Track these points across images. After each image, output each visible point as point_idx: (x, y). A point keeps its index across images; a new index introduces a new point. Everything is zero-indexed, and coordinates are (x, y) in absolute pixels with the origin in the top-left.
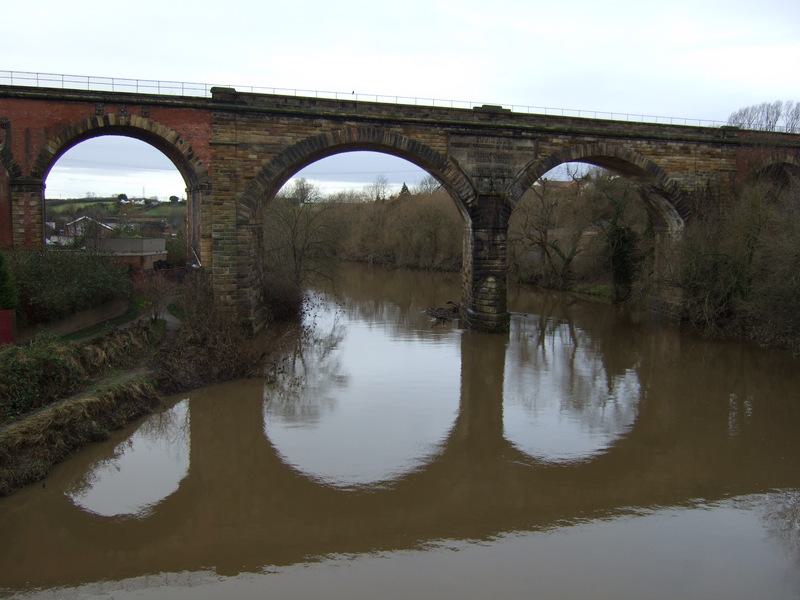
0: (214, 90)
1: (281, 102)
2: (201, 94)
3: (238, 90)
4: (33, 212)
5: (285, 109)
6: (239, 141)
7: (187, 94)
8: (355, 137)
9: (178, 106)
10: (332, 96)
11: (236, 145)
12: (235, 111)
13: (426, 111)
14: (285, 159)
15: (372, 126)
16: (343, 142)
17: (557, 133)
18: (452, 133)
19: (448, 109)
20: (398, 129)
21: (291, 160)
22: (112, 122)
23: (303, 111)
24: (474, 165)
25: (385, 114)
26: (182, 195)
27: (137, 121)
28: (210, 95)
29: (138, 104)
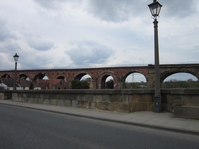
0: (148, 65)
1: (163, 66)
2: (147, 66)
3: (152, 64)
4: (121, 85)
5: (161, 67)
6: (153, 72)
7: (144, 66)
8: (175, 71)
9: (142, 68)
10: (170, 64)
11: (152, 73)
12: (152, 68)
13: (190, 65)
14: (161, 75)
15: (178, 69)
16: (172, 71)
17: (9, 92)
18: (196, 68)
19: (195, 64)
20: (184, 69)
21: (97, 87)
22: (132, 71)
23: (164, 67)
24: (88, 104)
25: (131, 67)
26: (145, 81)
27: (189, 69)
28: (148, 66)
29: (136, 68)
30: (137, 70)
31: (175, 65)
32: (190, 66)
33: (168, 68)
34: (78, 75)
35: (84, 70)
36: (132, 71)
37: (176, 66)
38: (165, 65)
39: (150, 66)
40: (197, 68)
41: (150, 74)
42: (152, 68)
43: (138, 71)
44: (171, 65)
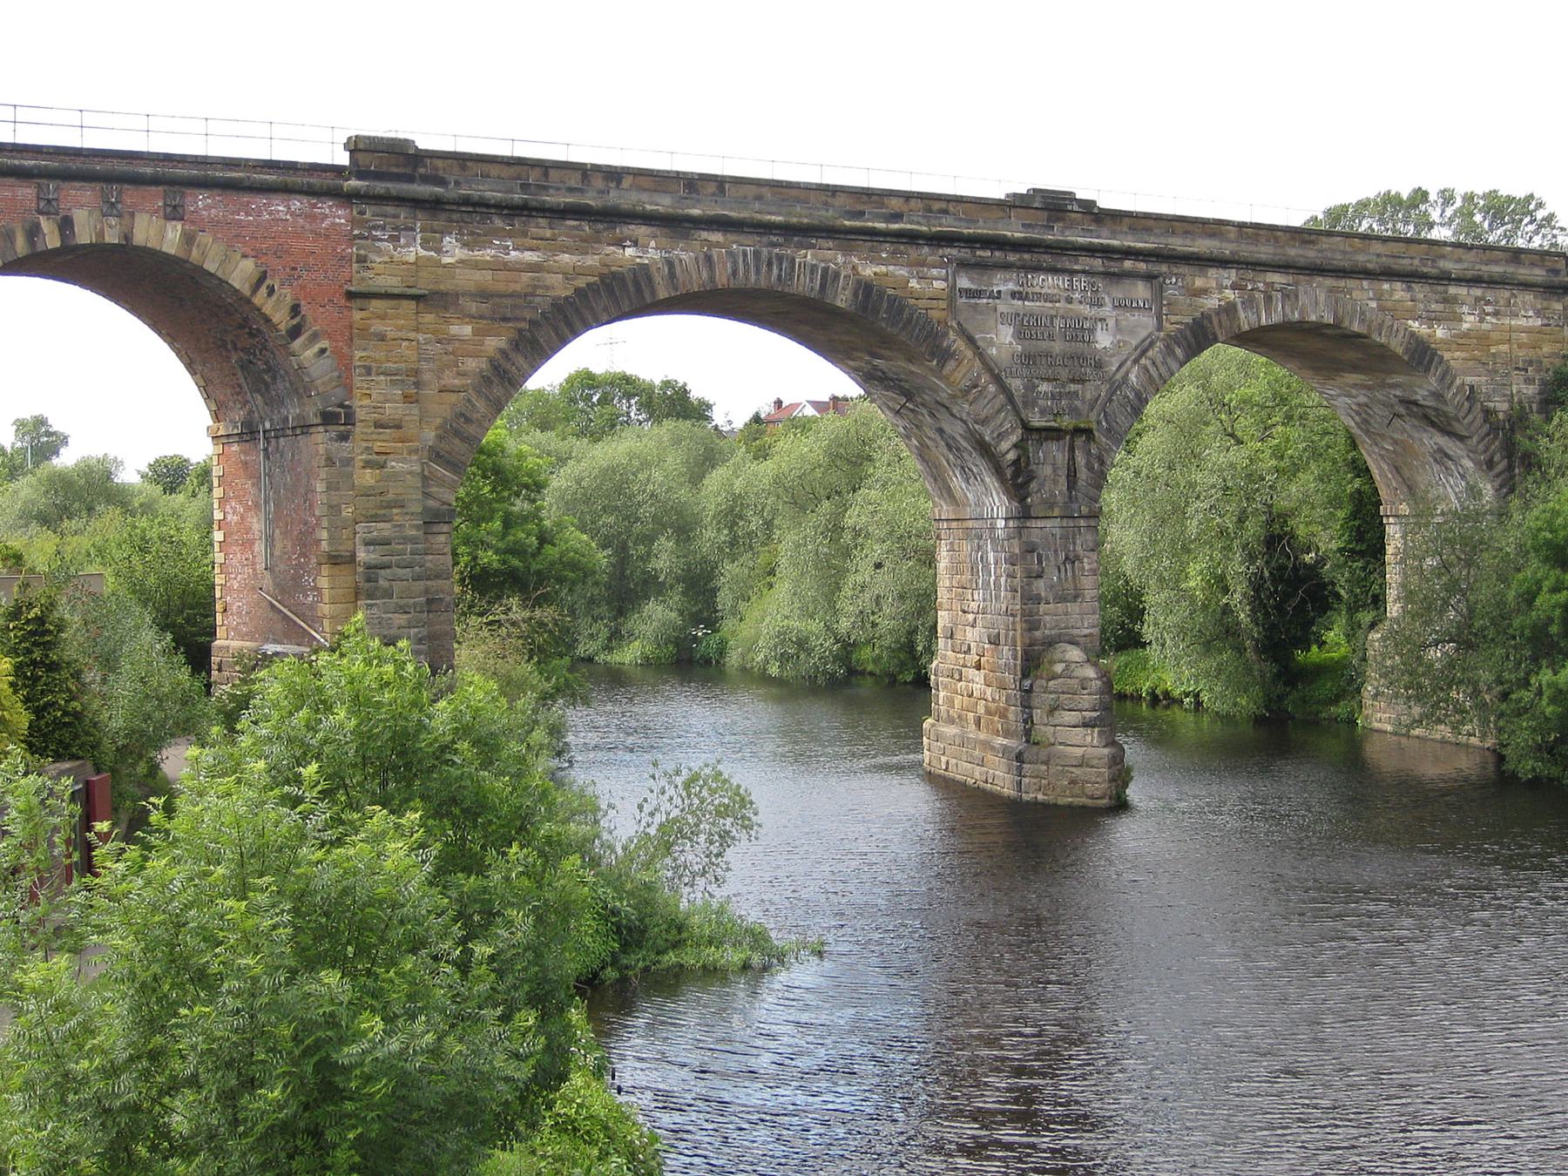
12: (416, 203)
13: (895, 203)
28: (343, 159)
29: (155, 181)
30: (174, 213)
31: (720, 184)
32: (897, 217)
33: (641, 231)
34: (392, 139)
35: (1297, 268)
36: (66, 225)
37: (743, 202)
38: (596, 168)
39: (378, 176)
40: (965, 254)
41: (377, 305)
42: (416, 203)
43: (188, 239)
44: (678, 177)
